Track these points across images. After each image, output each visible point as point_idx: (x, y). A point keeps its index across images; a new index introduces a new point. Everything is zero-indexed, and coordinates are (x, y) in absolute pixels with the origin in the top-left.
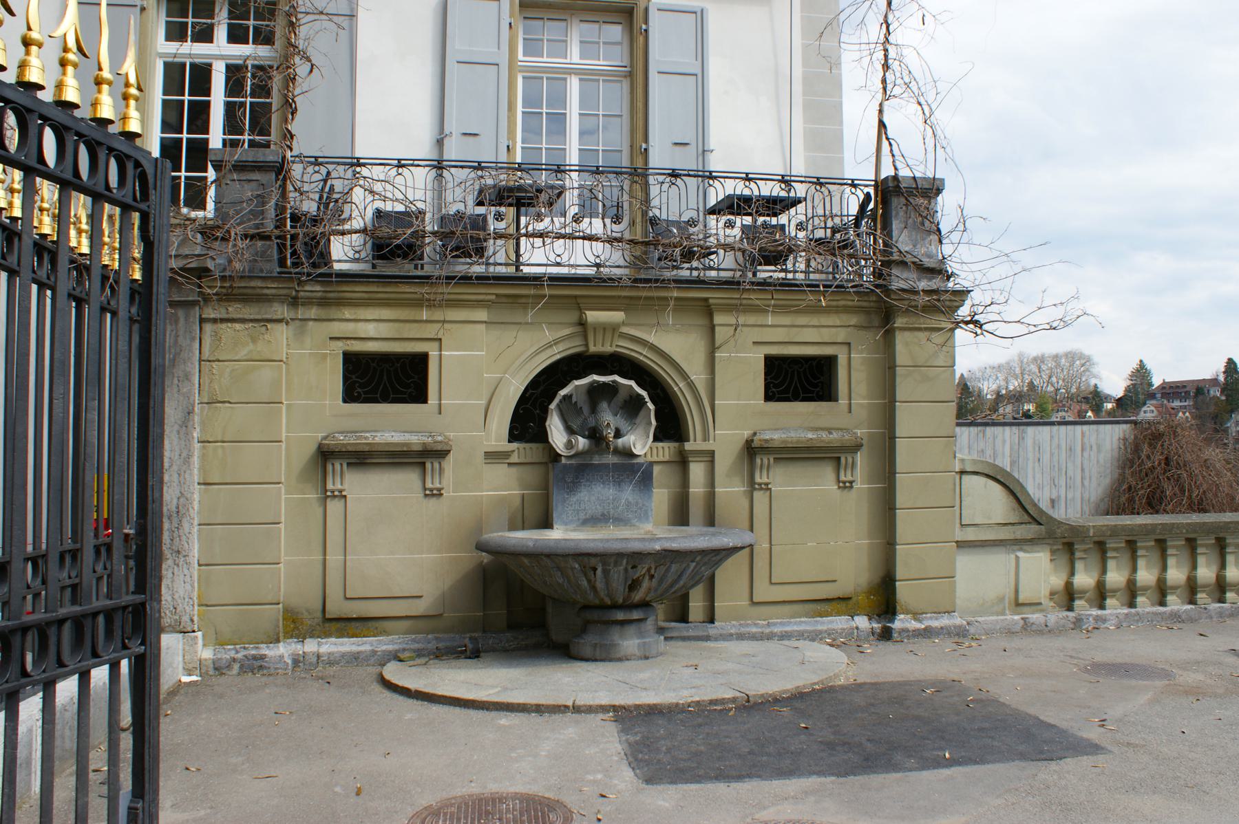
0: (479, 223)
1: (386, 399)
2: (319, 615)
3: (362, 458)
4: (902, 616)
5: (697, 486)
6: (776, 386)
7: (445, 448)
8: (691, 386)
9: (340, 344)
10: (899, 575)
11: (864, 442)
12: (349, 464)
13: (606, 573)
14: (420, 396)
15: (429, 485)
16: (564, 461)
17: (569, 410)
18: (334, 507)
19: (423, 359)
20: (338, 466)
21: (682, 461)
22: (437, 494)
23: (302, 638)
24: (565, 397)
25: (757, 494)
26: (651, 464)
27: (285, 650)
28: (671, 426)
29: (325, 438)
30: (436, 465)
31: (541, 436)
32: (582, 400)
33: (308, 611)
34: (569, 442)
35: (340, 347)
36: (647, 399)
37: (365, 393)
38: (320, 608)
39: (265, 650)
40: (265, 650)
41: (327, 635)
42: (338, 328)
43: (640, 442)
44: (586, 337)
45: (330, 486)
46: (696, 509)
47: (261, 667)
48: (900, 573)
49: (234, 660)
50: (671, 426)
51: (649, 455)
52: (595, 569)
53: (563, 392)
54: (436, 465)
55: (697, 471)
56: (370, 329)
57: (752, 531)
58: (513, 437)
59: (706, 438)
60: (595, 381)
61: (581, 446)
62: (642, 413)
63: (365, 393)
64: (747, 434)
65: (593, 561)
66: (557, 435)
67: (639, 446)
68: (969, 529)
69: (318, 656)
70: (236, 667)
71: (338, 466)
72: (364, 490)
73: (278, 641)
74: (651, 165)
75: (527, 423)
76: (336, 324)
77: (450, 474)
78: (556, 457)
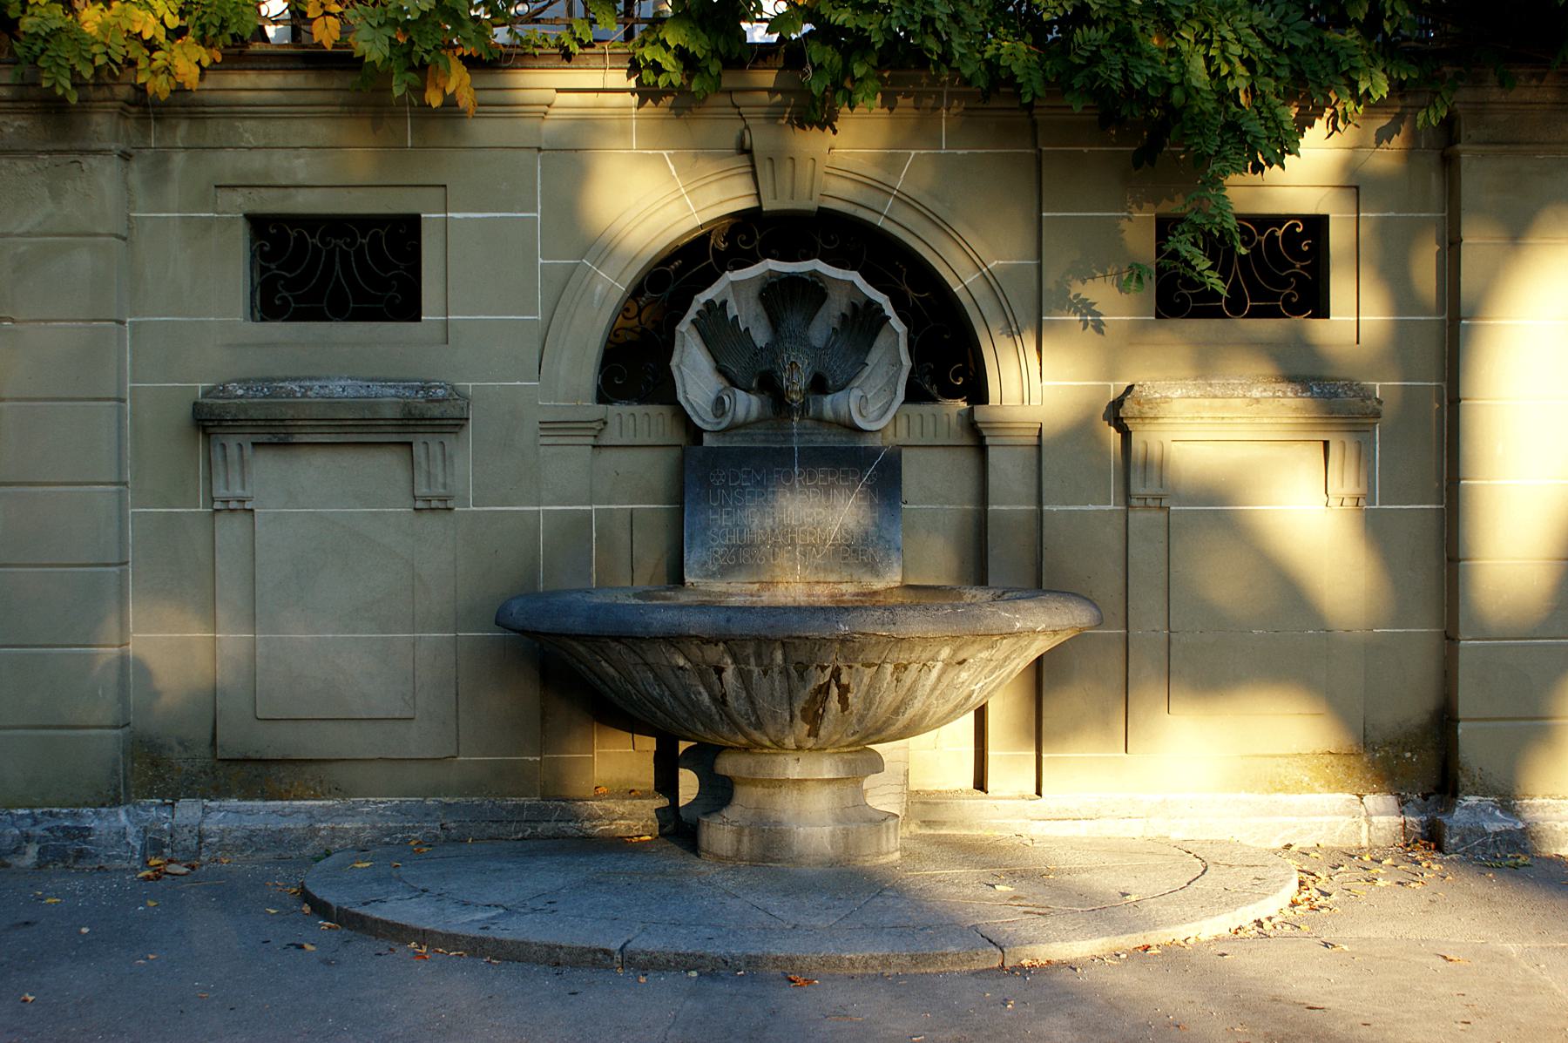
1: (340, 310)
3: (278, 431)
4: (1473, 800)
10: (1462, 713)
11: (1386, 410)
12: (254, 444)
13: (744, 676)
16: (708, 441)
18: (230, 530)
19: (411, 224)
20: (233, 451)
22: (438, 506)
23: (172, 794)
24: (709, 304)
25: (1137, 517)
27: (118, 823)
32: (747, 314)
34: (719, 401)
35: (240, 203)
36: (889, 310)
38: (208, 737)
39: (88, 817)
40: (88, 817)
41: (221, 792)
42: (229, 163)
45: (220, 491)
46: (1005, 553)
47: (81, 855)
48: (1464, 708)
49: (28, 838)
51: (890, 431)
52: (720, 671)
53: (701, 298)
54: (435, 448)
56: (301, 167)
61: (741, 413)
62: (882, 341)
65: (714, 653)
66: (695, 375)
69: (201, 836)
70: (32, 850)
72: (297, 494)
73: (116, 802)
77: (462, 465)
78: (694, 433)
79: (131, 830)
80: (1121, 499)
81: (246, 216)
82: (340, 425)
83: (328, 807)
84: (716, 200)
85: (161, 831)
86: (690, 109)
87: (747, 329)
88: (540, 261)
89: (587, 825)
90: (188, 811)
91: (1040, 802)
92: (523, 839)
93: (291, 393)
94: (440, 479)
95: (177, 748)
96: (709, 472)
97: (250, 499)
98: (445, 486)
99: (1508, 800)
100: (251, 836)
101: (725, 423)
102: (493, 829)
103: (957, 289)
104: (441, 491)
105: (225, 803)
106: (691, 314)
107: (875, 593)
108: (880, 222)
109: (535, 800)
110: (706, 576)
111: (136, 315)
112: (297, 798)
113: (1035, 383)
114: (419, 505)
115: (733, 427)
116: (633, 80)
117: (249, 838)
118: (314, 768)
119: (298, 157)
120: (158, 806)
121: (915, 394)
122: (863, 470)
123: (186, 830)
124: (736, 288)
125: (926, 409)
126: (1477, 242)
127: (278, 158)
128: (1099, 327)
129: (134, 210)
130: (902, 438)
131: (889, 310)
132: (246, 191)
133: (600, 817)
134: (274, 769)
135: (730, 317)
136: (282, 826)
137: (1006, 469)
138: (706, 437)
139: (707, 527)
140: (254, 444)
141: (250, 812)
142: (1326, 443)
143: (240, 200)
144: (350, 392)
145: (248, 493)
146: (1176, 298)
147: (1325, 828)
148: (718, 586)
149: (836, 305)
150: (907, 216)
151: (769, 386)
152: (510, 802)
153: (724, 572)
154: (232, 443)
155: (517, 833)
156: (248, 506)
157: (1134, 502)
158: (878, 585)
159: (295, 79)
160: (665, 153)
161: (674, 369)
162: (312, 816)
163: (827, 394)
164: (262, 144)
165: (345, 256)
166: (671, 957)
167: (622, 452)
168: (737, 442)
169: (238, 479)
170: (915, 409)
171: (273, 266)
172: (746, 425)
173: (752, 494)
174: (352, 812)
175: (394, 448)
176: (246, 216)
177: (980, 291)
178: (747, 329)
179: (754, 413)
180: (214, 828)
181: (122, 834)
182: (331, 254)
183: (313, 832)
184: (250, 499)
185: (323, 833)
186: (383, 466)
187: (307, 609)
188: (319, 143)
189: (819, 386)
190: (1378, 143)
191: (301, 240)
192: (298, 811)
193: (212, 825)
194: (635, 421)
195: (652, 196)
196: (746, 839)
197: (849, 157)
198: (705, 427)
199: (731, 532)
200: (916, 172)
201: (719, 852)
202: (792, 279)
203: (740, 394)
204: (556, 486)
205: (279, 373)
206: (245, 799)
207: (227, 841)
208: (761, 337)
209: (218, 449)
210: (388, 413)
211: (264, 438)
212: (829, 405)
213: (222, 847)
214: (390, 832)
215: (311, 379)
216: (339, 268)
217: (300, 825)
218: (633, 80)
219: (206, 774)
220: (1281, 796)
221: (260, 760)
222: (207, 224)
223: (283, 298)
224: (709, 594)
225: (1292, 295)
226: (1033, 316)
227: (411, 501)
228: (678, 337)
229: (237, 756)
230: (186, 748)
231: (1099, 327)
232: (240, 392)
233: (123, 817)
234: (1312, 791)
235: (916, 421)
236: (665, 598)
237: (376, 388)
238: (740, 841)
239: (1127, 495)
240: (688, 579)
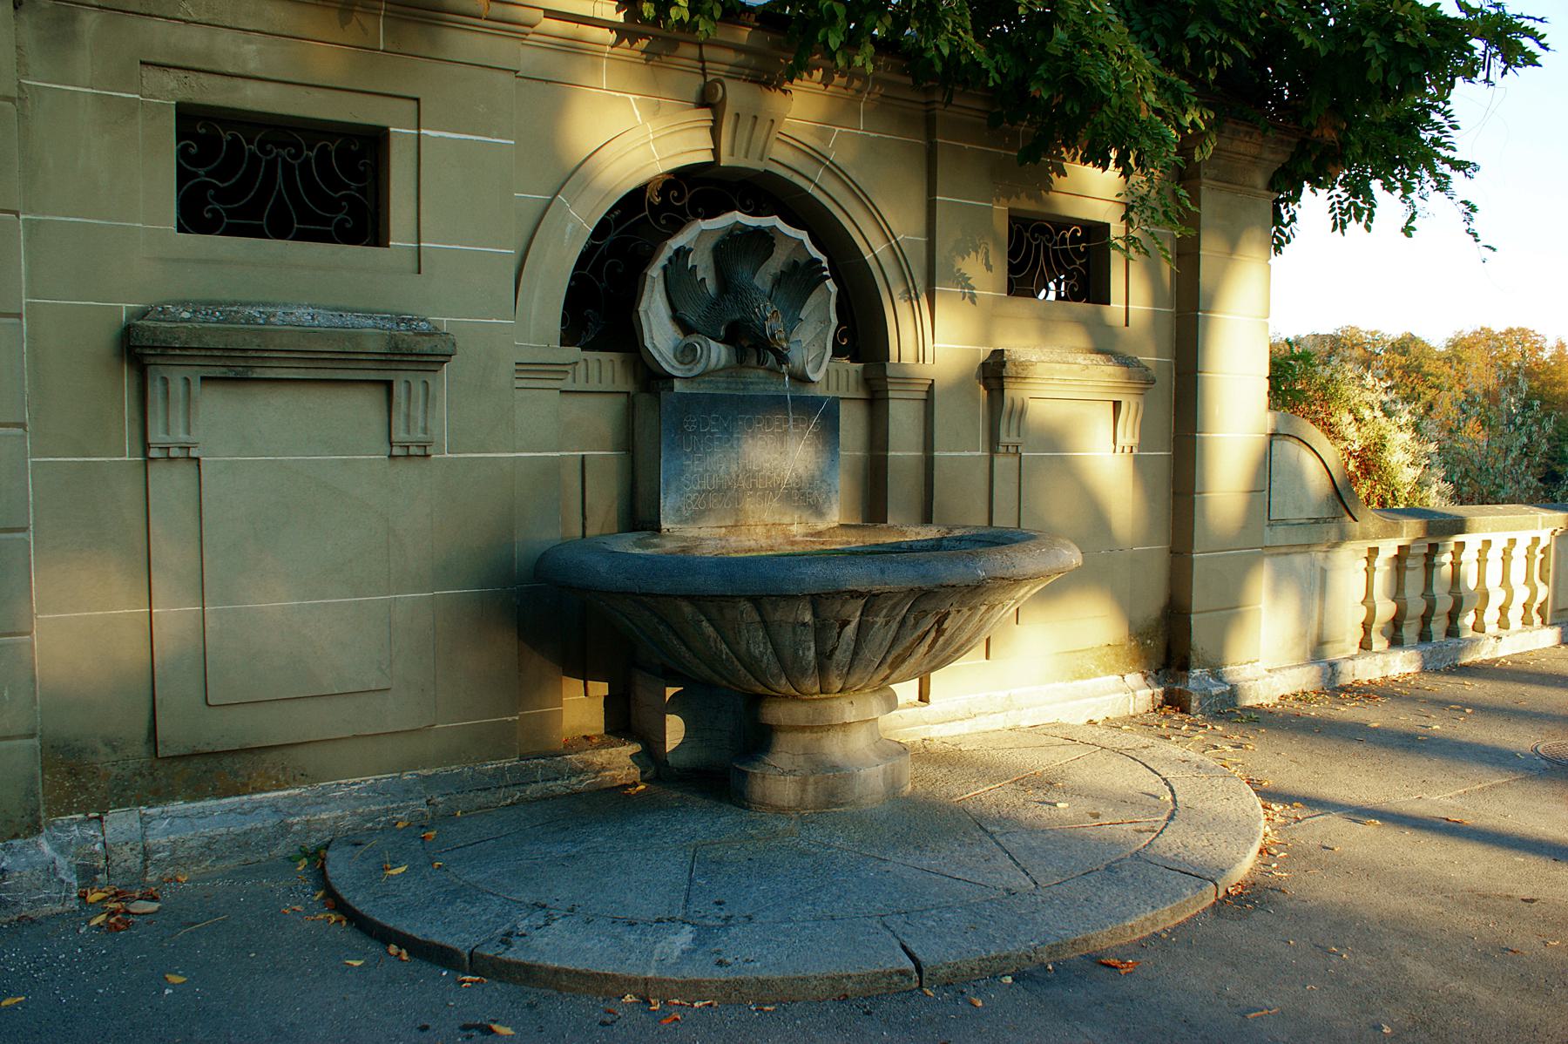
0: (1459, 498)
1: (280, 230)
2: (140, 749)
3: (238, 362)
4: (1197, 672)
5: (903, 449)
6: (221, 196)
7: (442, 347)
9: (170, 80)
12: (203, 379)
14: (367, 227)
15: (399, 435)
16: (678, 386)
18: (169, 483)
19: (374, 141)
20: (177, 387)
23: (98, 809)
25: (999, 461)
26: (836, 400)
29: (144, 314)
30: (418, 389)
32: (702, 263)
33: (108, 743)
35: (173, 89)
37: (231, 213)
38: (142, 730)
41: (161, 795)
45: (156, 435)
54: (418, 389)
57: (987, 657)
58: (568, 339)
63: (231, 213)
68: (1280, 529)
69: (146, 853)
71: (177, 387)
73: (35, 829)
76: (158, 25)
79: (61, 862)
80: (987, 447)
82: (313, 358)
84: (678, 150)
85: (93, 854)
86: (659, 55)
89: (574, 780)
90: (121, 823)
91: (924, 710)
92: (512, 804)
93: (250, 320)
94: (420, 424)
95: (103, 750)
96: (658, 422)
97: (195, 445)
98: (425, 430)
99: (1217, 673)
100: (209, 844)
102: (482, 798)
103: (868, 257)
104: (420, 436)
105: (170, 808)
107: (819, 534)
108: (811, 189)
109: (515, 761)
110: (680, 522)
111: (32, 211)
112: (256, 790)
113: (936, 340)
114: (396, 451)
116: (622, 14)
117: (208, 846)
118: (274, 755)
119: (249, 42)
120: (80, 823)
122: (810, 418)
123: (127, 849)
124: (697, 236)
126: (1210, 248)
127: (224, 39)
128: (973, 298)
129: (27, 76)
132: (182, 74)
133: (582, 771)
134: (227, 761)
136: (248, 827)
137: (903, 416)
138: (677, 383)
139: (681, 473)
140: (203, 379)
141: (202, 815)
142: (1117, 405)
143: (173, 84)
144: (320, 320)
145: (192, 439)
146: (1021, 281)
148: (691, 531)
149: (777, 262)
150: (834, 187)
152: (490, 766)
153: (696, 517)
154: (176, 377)
156: (193, 453)
157: (153, 453)
158: (821, 526)
160: (631, 97)
161: (642, 314)
162: (277, 811)
164: (204, 18)
165: (288, 169)
166: (975, 964)
168: (702, 389)
169: (181, 421)
171: (201, 172)
172: (714, 371)
173: (719, 439)
174: (323, 800)
175: (366, 387)
177: (886, 259)
179: (723, 361)
180: (163, 841)
181: (51, 870)
182: (271, 166)
183: (285, 829)
184: (195, 445)
186: (361, 406)
187: (284, 574)
188: (277, 30)
190: (1065, 175)
191: (235, 144)
192: (259, 806)
193: (159, 836)
195: (632, 134)
196: (810, 788)
197: (801, 121)
198: (675, 373)
199: (702, 477)
200: (843, 146)
201: (780, 803)
202: (758, 231)
204: (522, 433)
205: (226, 297)
206: (193, 799)
207: (180, 854)
209: (158, 383)
210: (372, 346)
211: (217, 372)
213: (175, 861)
214: (372, 817)
215: (273, 305)
216: (284, 177)
217: (270, 822)
218: (622, 14)
219: (141, 774)
220: (1079, 682)
222: (130, 108)
223: (213, 211)
224: (685, 539)
226: (928, 283)
227: (386, 448)
229: (183, 751)
230: (114, 749)
231: (973, 298)
232: (186, 315)
233: (46, 848)
234: (1096, 676)
236: (656, 546)
237: (349, 319)
238: (804, 790)
239: (146, 446)
240: (664, 525)
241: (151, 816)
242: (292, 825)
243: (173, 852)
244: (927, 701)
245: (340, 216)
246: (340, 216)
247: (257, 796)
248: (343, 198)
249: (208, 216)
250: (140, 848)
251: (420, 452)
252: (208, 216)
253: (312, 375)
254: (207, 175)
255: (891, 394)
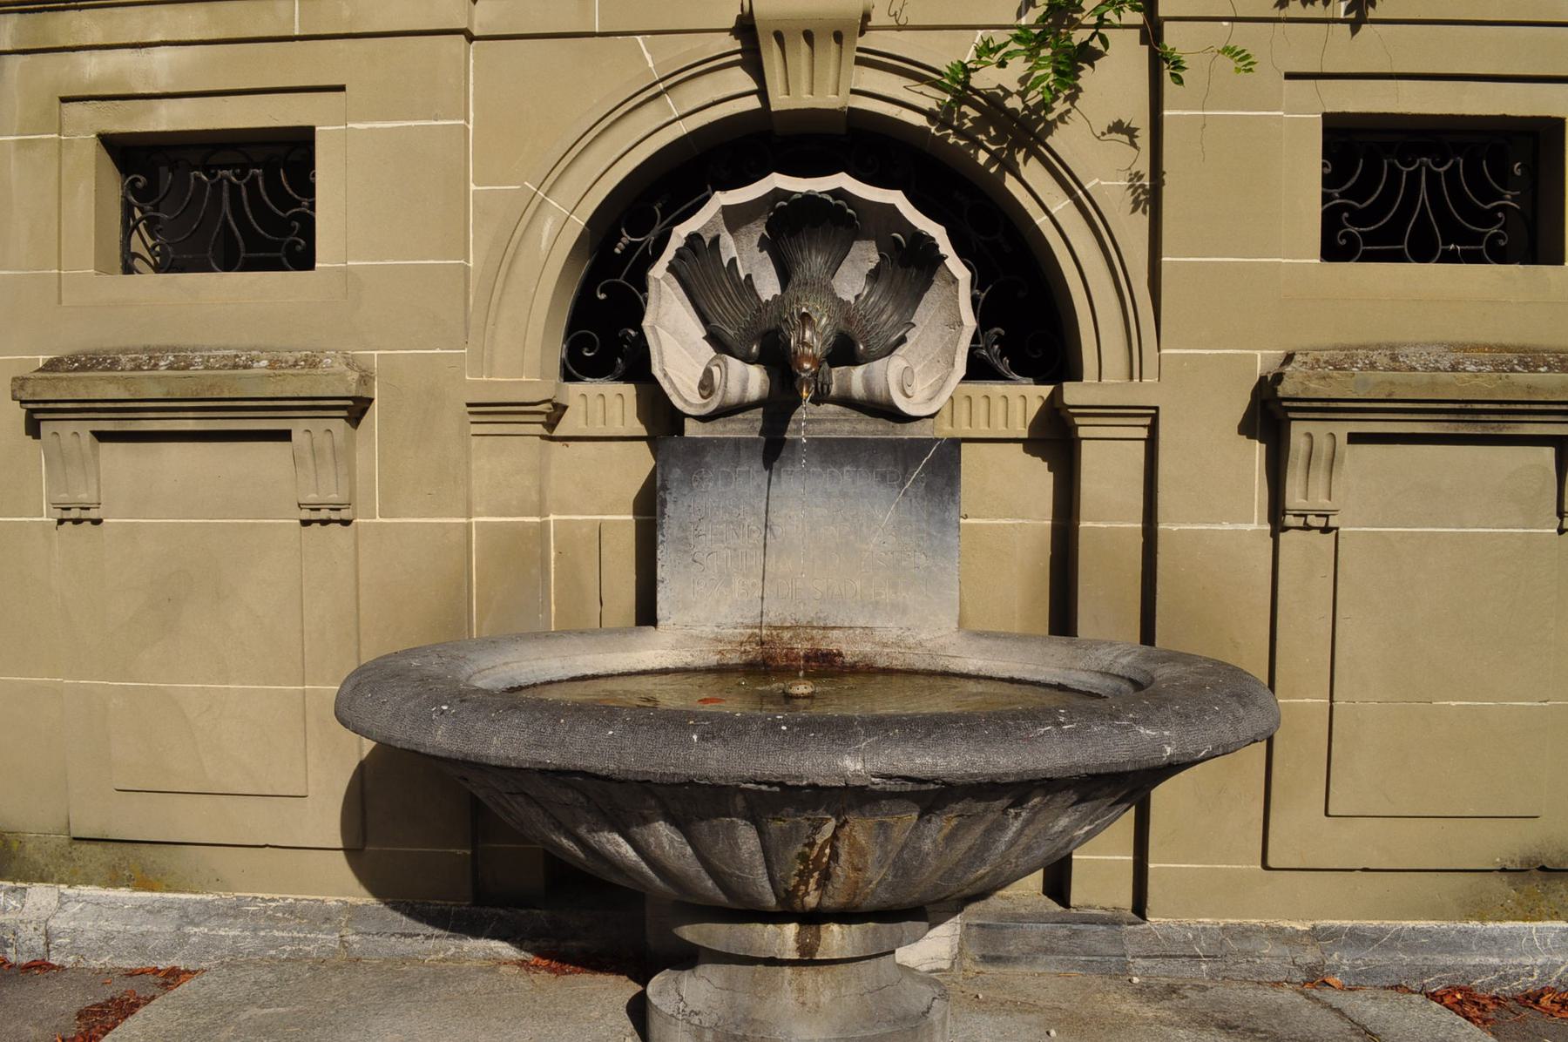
1: (1423, 253)
5: (1109, 510)
6: (1358, 218)
8: (1086, 207)
16: (692, 429)
17: (702, 272)
21: (1055, 439)
24: (694, 238)
26: (956, 443)
28: (1028, 327)
31: (632, 363)
36: (945, 247)
43: (925, 370)
44: (755, 67)
45: (1294, 498)
50: (1028, 327)
53: (680, 233)
55: (1108, 465)
59: (1133, 370)
60: (777, 193)
62: (933, 297)
64: (1262, 360)
67: (920, 389)
74: (1049, 140)
75: (603, 334)
81: (99, 135)
83: (206, 904)
87: (749, 277)
88: (472, 187)
101: (713, 404)
106: (669, 254)
115: (726, 412)
121: (978, 369)
123: (31, 927)
125: (996, 388)
130: (963, 430)
131: (945, 247)
135: (743, 277)
138: (688, 423)
147: (1536, 972)
151: (775, 355)
155: (437, 952)
157: (1290, 520)
159: (837, 408)
163: (857, 364)
165: (234, 189)
167: (1339, 585)
170: (978, 389)
176: (99, 135)
178: (749, 277)
185: (194, 939)
189: (844, 352)
194: (607, 404)
203: (735, 364)
208: (768, 286)
212: (856, 379)
221: (573, 679)
223: (1348, 235)
225: (1496, 236)
228: (652, 286)
235: (981, 407)
241: (68, 897)
242: (190, 936)
243: (74, 941)
244: (1144, 918)
245: (1494, 230)
246: (1494, 230)
247: (170, 896)
248: (295, 217)
249: (1344, 242)
250: (42, 929)
251: (1321, 522)
252: (1344, 242)
253: (1477, 430)
254: (1342, 196)
255: (1082, 432)
